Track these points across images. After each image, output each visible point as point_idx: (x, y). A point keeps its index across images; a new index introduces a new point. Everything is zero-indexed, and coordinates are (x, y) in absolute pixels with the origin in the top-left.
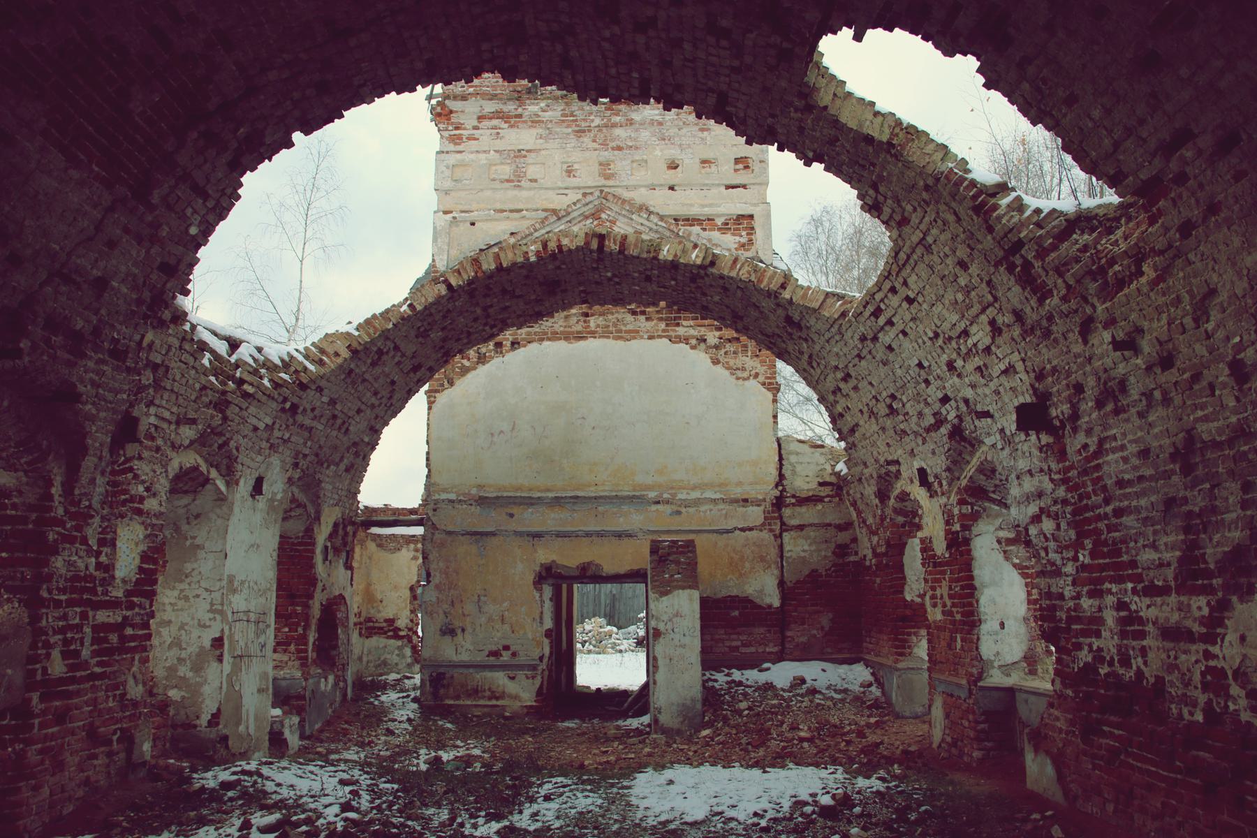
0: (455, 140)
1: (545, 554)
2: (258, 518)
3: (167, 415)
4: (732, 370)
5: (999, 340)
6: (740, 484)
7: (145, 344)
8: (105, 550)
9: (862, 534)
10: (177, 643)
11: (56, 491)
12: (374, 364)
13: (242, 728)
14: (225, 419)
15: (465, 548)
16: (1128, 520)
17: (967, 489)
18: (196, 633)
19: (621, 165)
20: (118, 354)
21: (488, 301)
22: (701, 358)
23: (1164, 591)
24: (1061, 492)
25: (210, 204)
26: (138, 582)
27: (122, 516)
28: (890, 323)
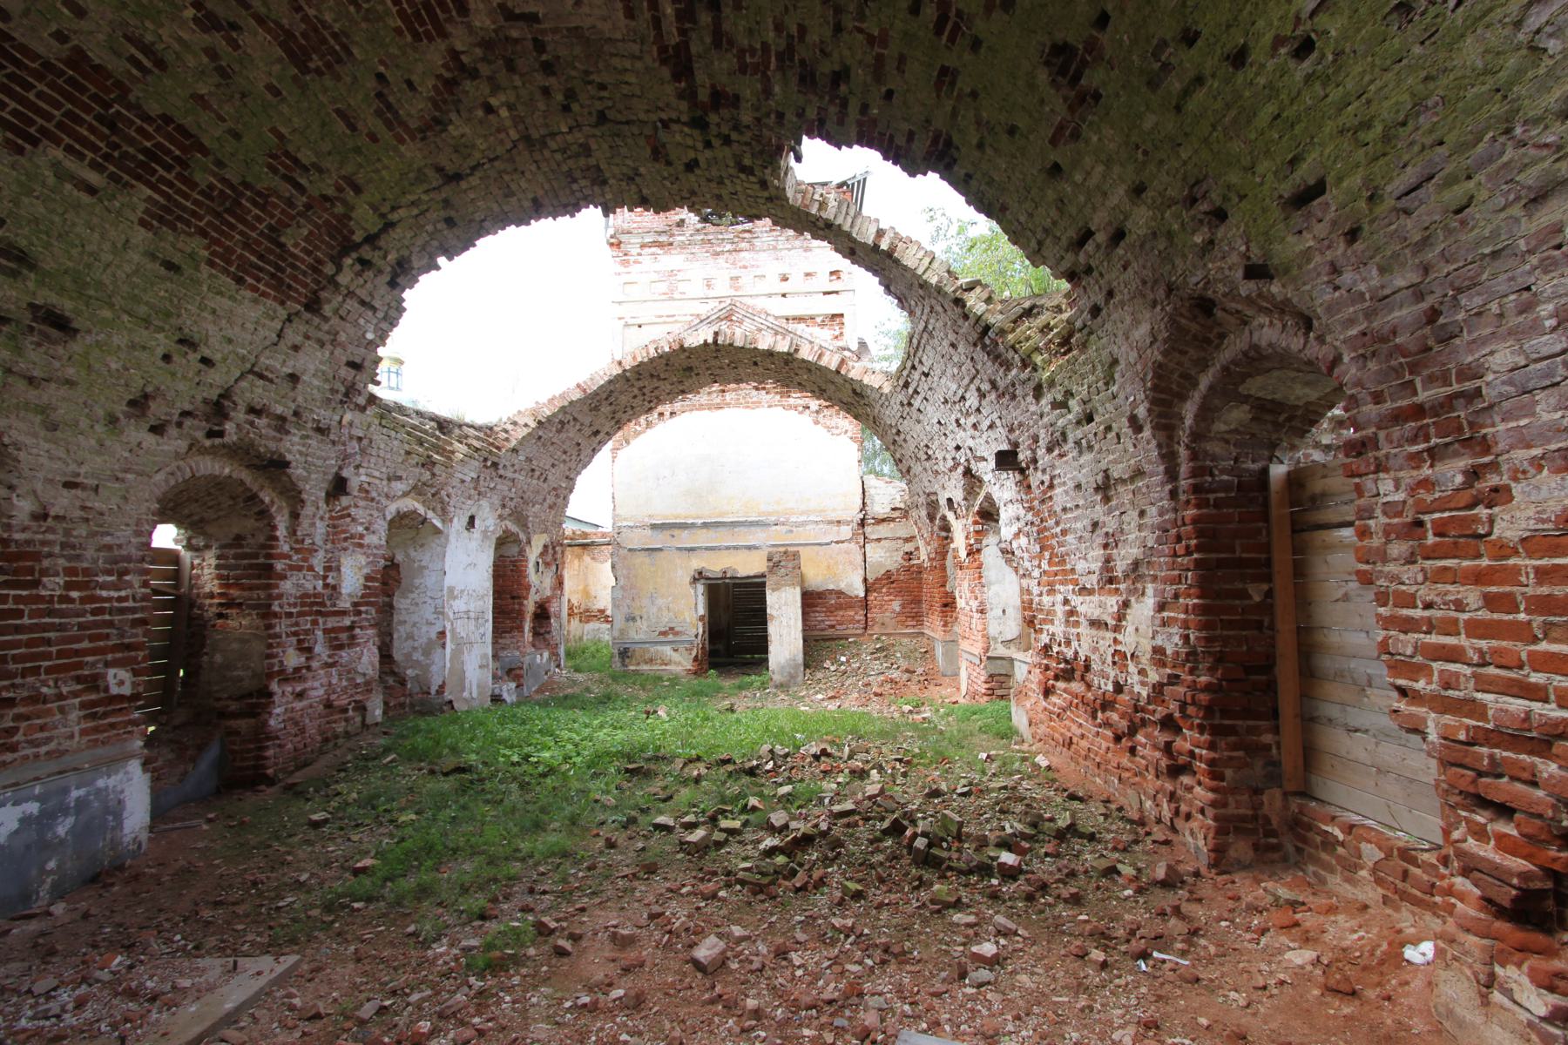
0: (625, 263)
1: (696, 563)
2: (474, 545)
3: (377, 474)
4: (829, 428)
5: (984, 403)
6: (834, 510)
7: (344, 422)
8: (331, 574)
9: (921, 543)
10: (410, 637)
11: (281, 532)
12: (559, 431)
13: (466, 694)
14: (434, 475)
15: (642, 558)
16: (1070, 538)
17: (978, 513)
18: (424, 629)
19: (746, 279)
20: (321, 431)
21: (641, 384)
22: (806, 419)
23: (1090, 592)
24: (1030, 517)
25: (380, 315)
26: (363, 596)
27: (345, 549)
28: (916, 392)
